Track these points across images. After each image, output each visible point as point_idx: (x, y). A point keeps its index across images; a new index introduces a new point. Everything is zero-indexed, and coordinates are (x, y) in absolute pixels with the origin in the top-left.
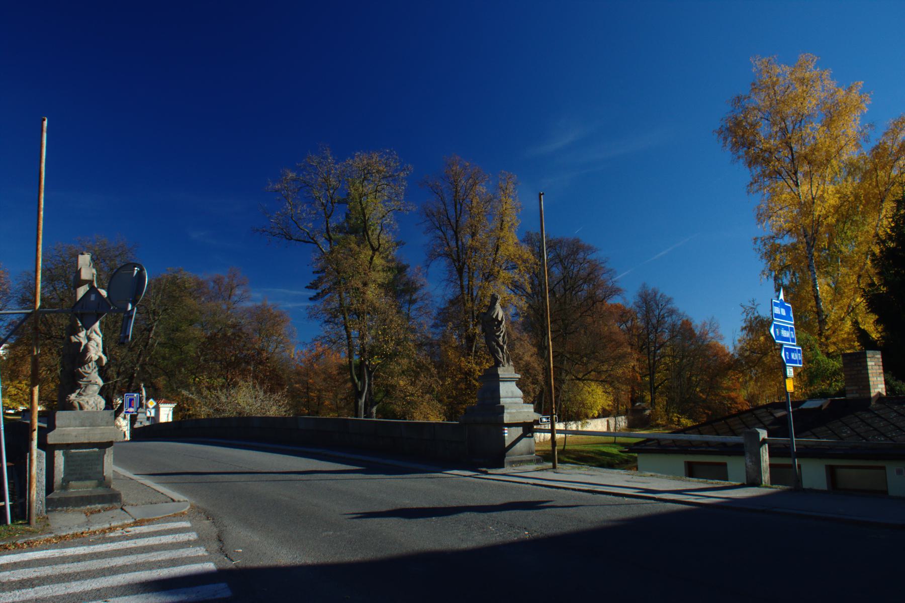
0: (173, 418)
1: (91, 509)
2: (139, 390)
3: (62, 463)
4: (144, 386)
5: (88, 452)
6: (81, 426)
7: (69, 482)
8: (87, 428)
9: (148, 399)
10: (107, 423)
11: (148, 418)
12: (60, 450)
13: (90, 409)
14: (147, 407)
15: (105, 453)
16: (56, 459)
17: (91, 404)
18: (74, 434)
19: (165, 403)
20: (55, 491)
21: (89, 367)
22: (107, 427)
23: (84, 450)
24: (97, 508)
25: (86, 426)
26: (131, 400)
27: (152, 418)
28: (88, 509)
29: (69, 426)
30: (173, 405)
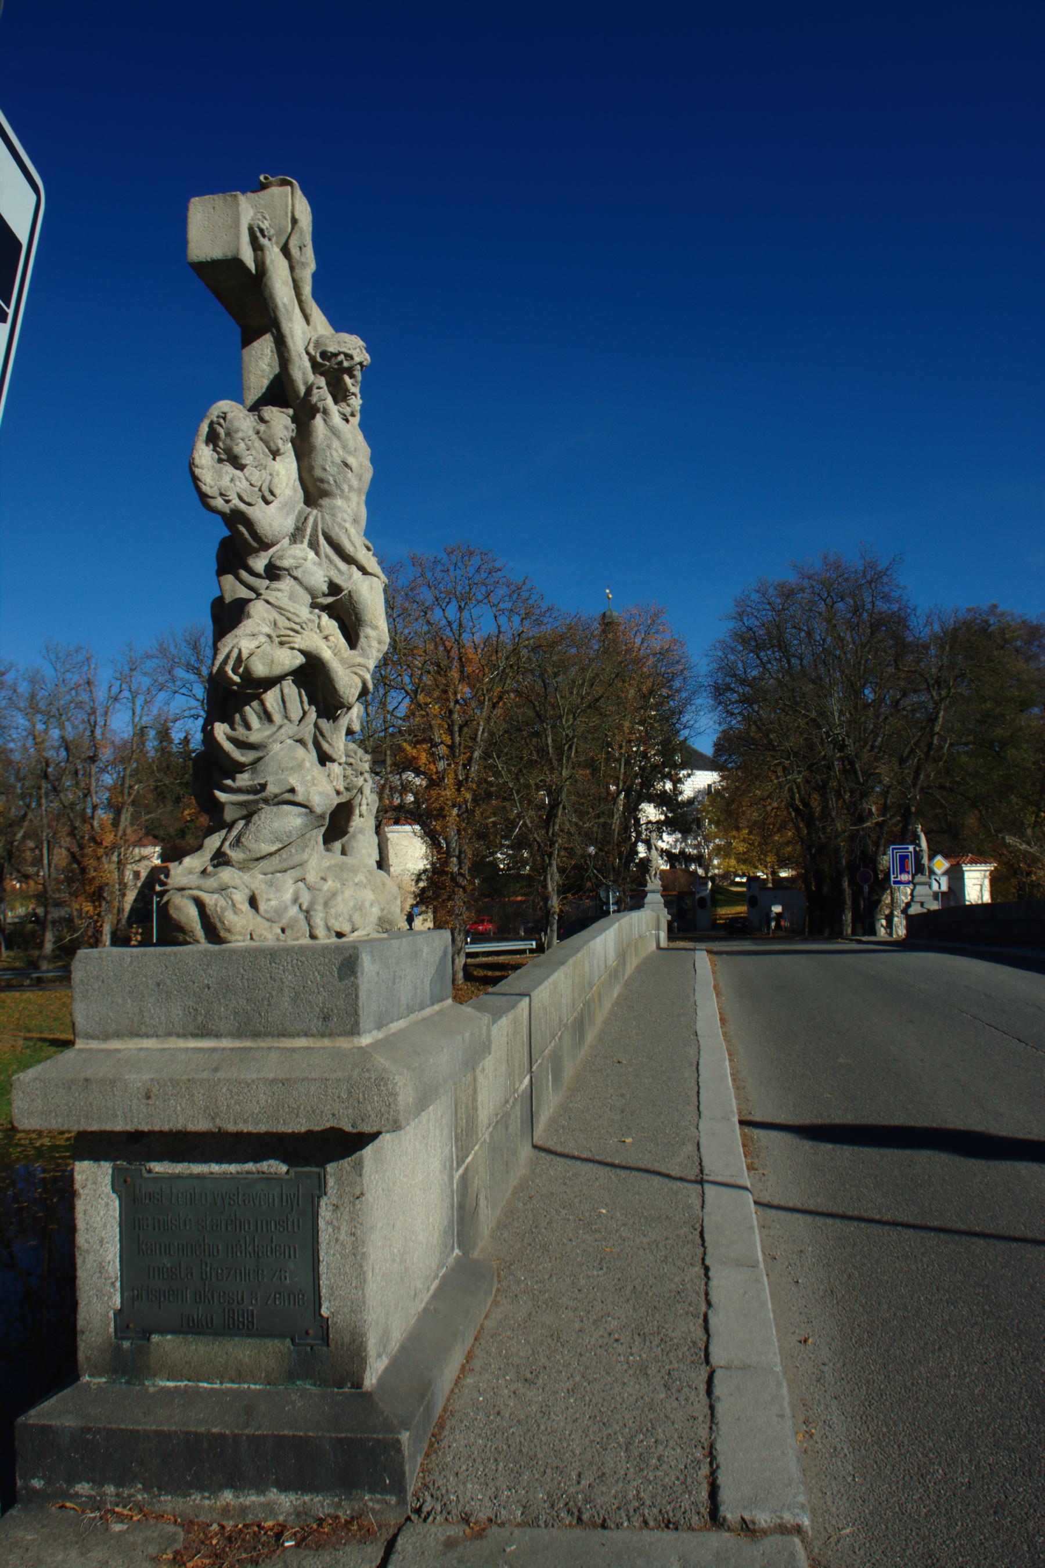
0: (993, 894)
1: (243, 1510)
2: (915, 840)
3: (113, 1232)
4: (922, 830)
5: (233, 1178)
6: (195, 1036)
7: (146, 1335)
8: (226, 1043)
9: (931, 858)
10: (326, 1018)
11: (936, 896)
12: (96, 1158)
13: (269, 936)
14: (932, 872)
15: (321, 1188)
16: (80, 1206)
17: (280, 912)
18: (138, 1079)
19: (973, 862)
20: (86, 1378)
21: (267, 717)
22: (326, 1042)
23: (215, 1168)
24: (270, 1509)
25: (218, 1036)
26: (903, 859)
27: (943, 893)
28: (226, 1511)
29: (135, 1034)
30: (991, 867)
